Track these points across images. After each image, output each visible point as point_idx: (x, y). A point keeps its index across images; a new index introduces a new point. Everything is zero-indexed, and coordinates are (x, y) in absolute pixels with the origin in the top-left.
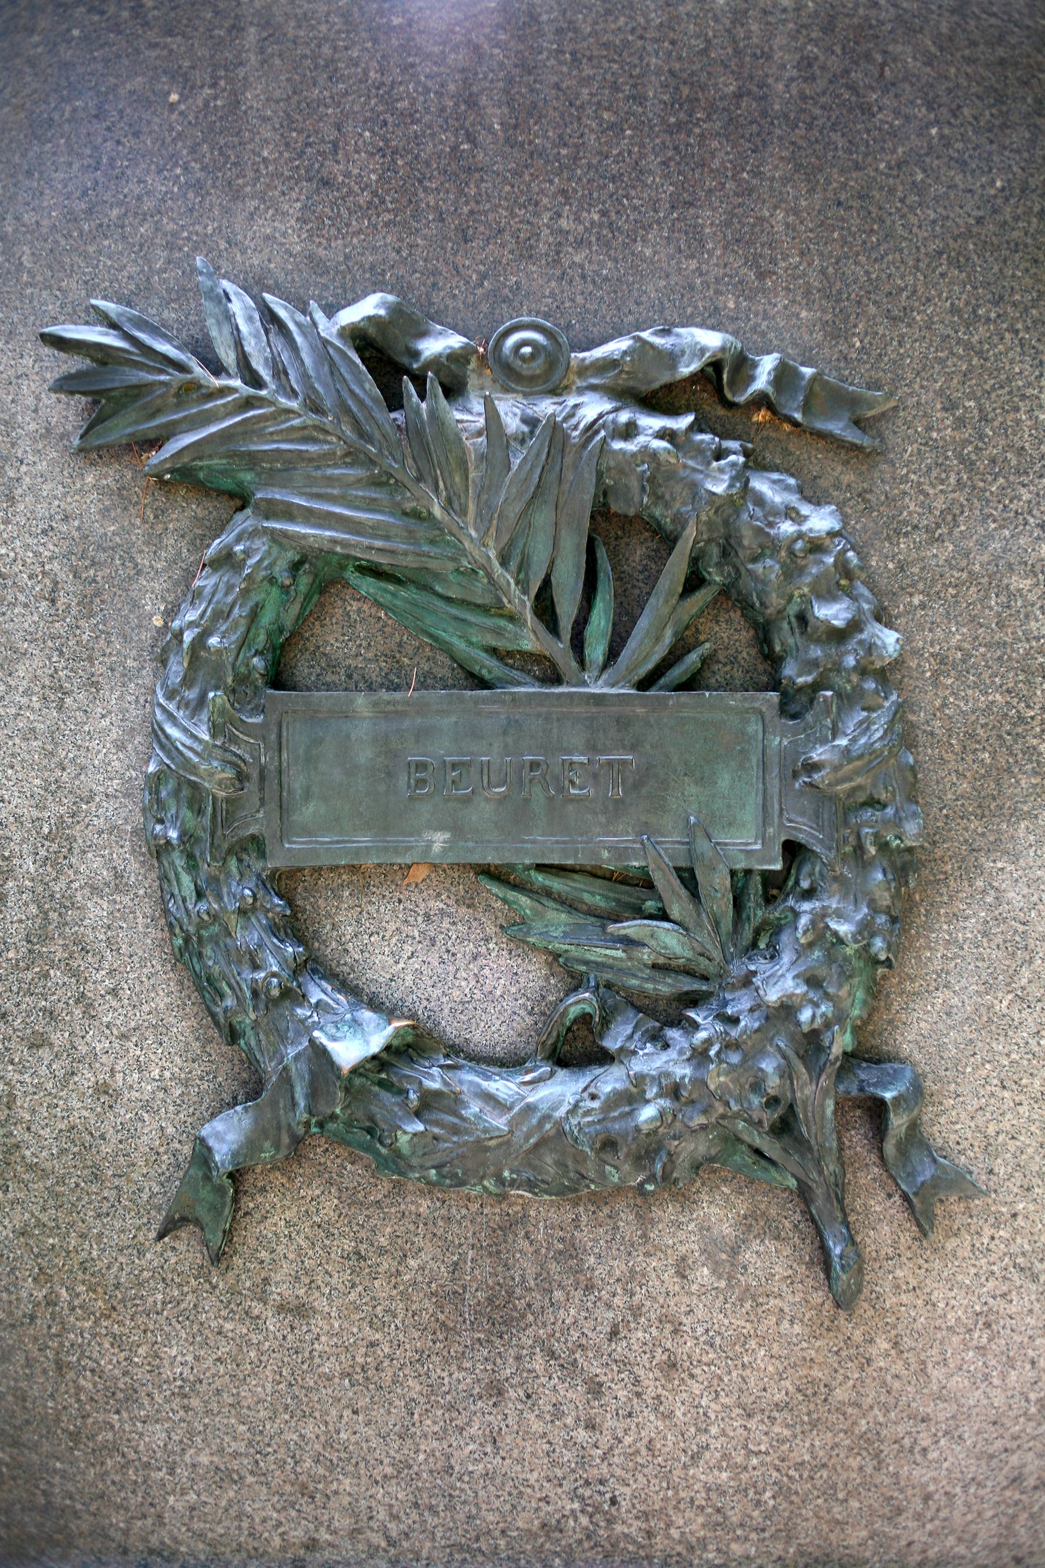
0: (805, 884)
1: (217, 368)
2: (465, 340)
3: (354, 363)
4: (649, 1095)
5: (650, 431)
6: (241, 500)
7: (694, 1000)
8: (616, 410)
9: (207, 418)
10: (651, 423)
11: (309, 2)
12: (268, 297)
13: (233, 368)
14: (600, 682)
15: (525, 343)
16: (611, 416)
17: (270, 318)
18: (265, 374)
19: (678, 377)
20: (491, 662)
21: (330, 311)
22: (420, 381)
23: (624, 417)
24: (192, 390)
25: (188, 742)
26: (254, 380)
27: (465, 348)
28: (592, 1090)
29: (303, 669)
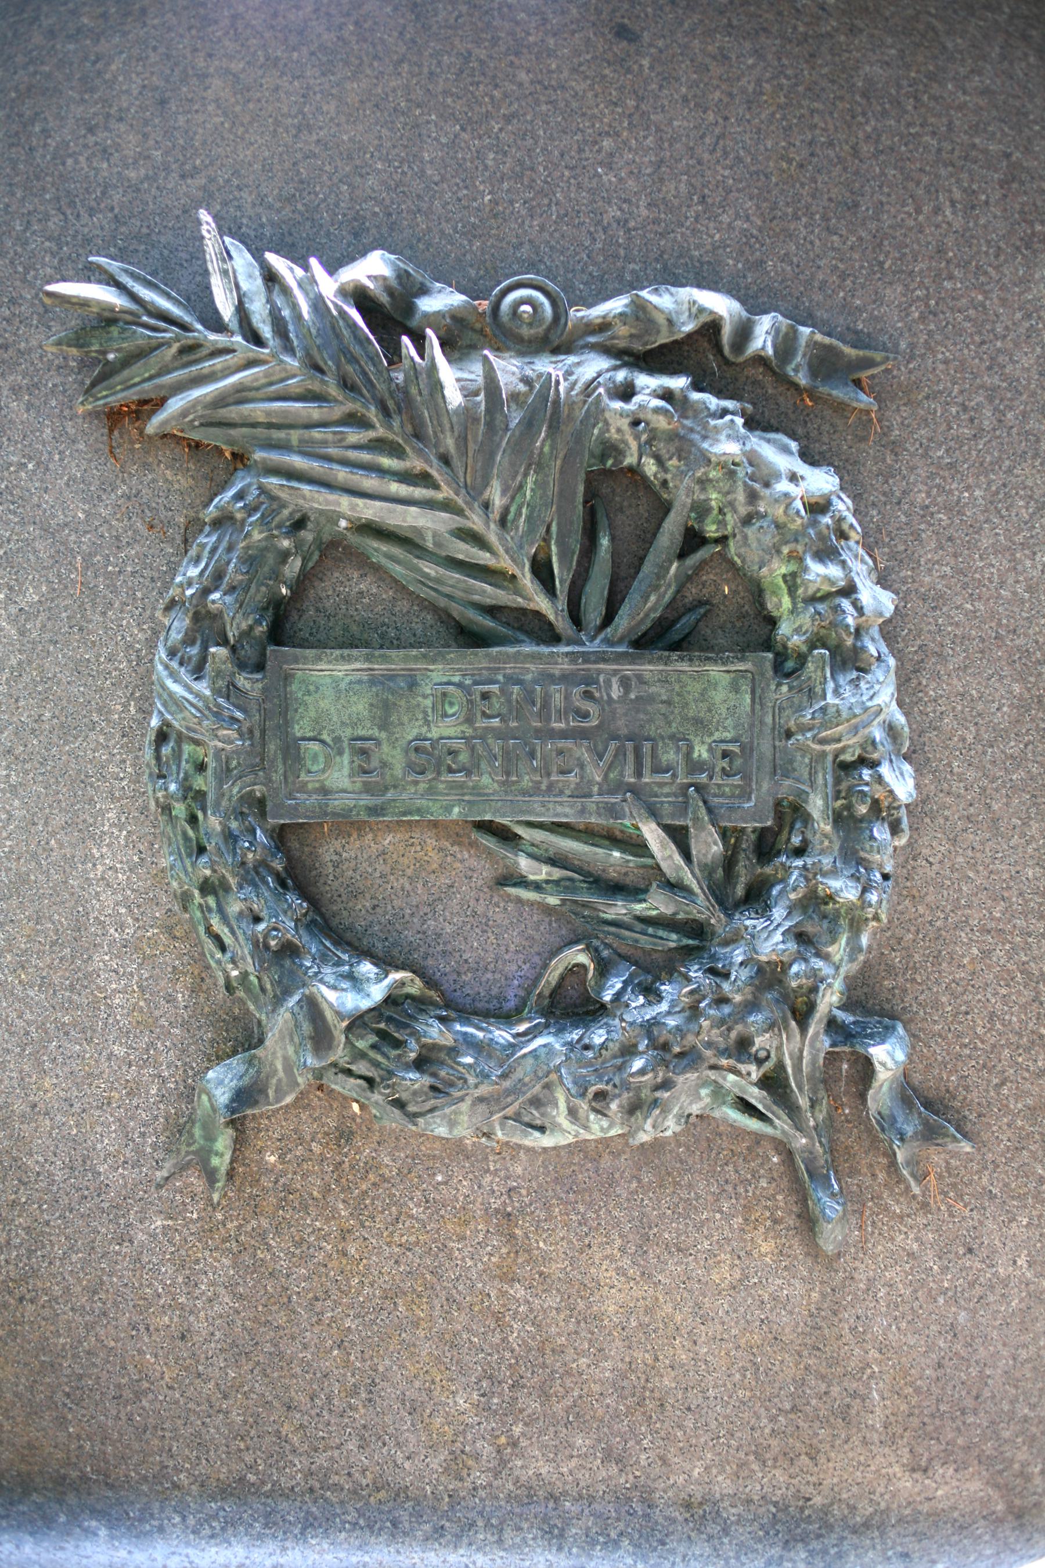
0: (796, 840)
1: (217, 325)
2: (463, 298)
3: (355, 325)
4: (641, 1047)
5: (647, 391)
6: (239, 458)
7: (688, 953)
8: (615, 368)
9: (210, 377)
10: (646, 382)
11: (365, 1565)
12: (271, 257)
13: (234, 325)
14: (597, 641)
15: (528, 301)
16: (608, 375)
17: (271, 278)
18: (266, 331)
19: (679, 337)
20: (489, 623)
21: (332, 269)
22: (419, 341)
23: (621, 375)
24: (190, 351)
25: (190, 697)
26: (256, 339)
27: (465, 307)
28: (587, 1041)
29: (302, 623)
